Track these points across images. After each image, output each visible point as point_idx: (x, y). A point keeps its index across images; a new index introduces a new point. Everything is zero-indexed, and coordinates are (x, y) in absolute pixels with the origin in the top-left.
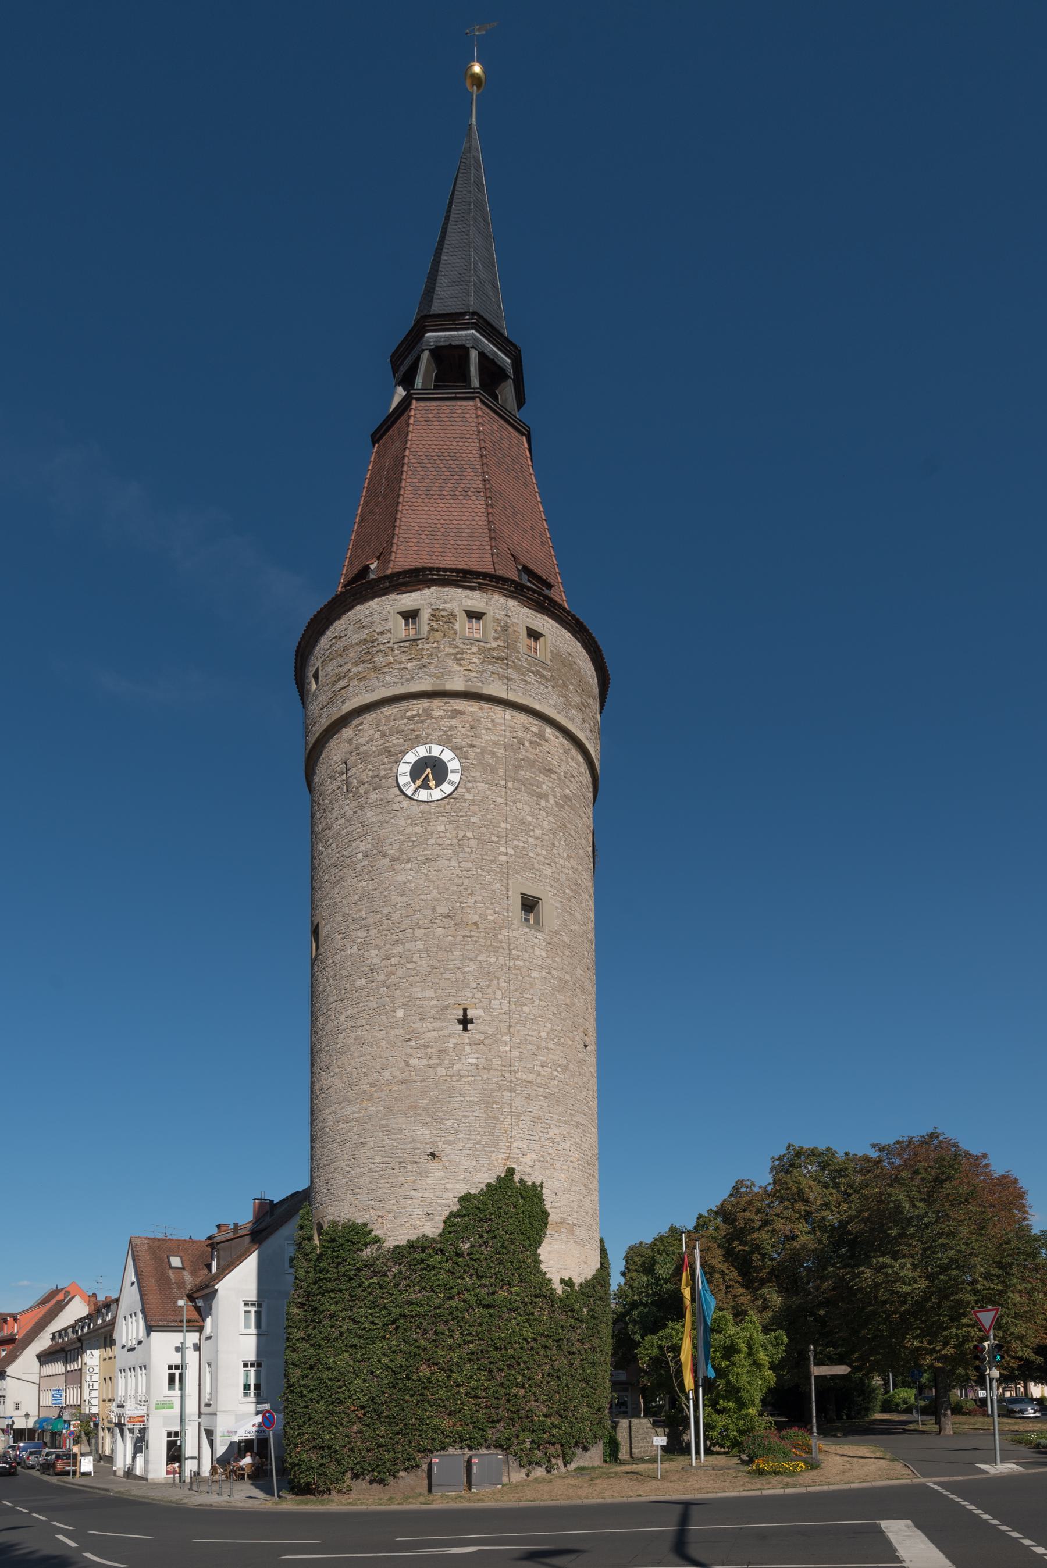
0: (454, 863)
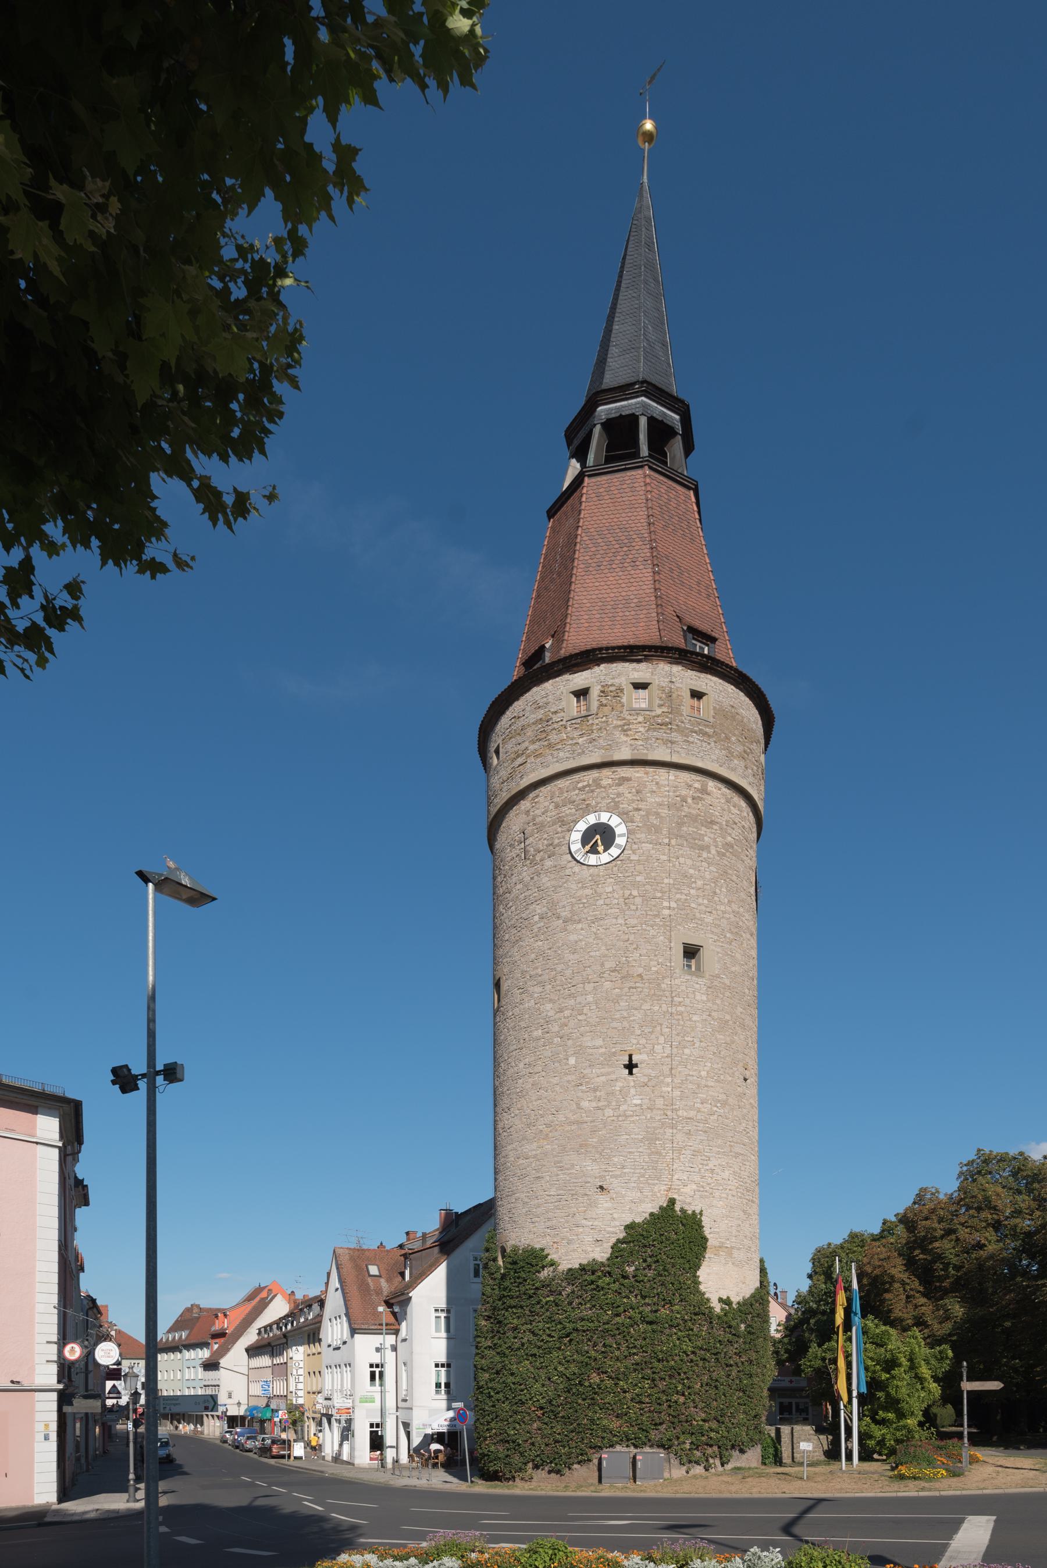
0: (621, 921)
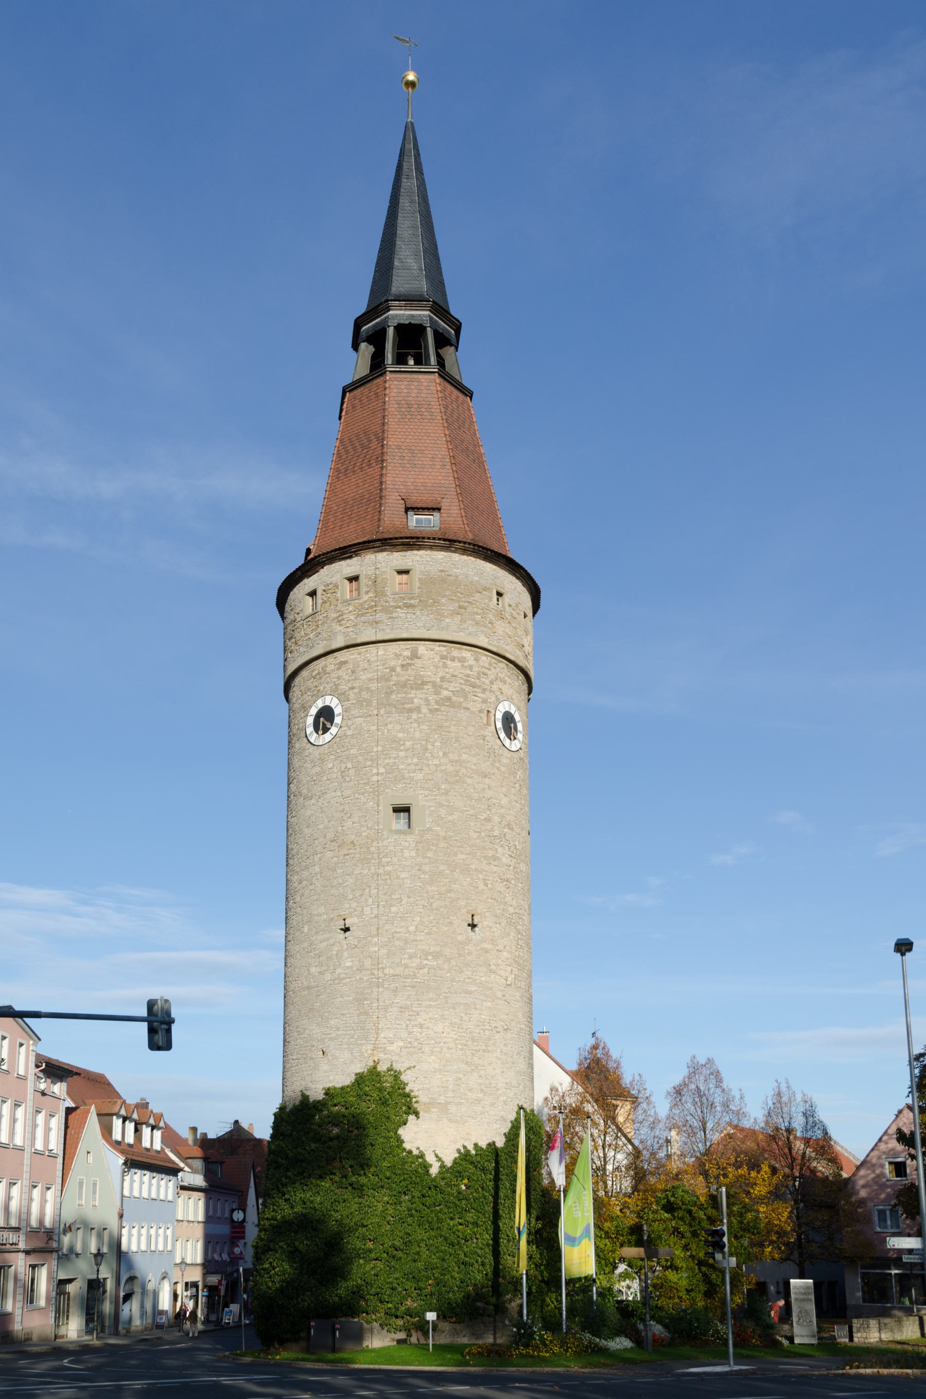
0: (339, 793)
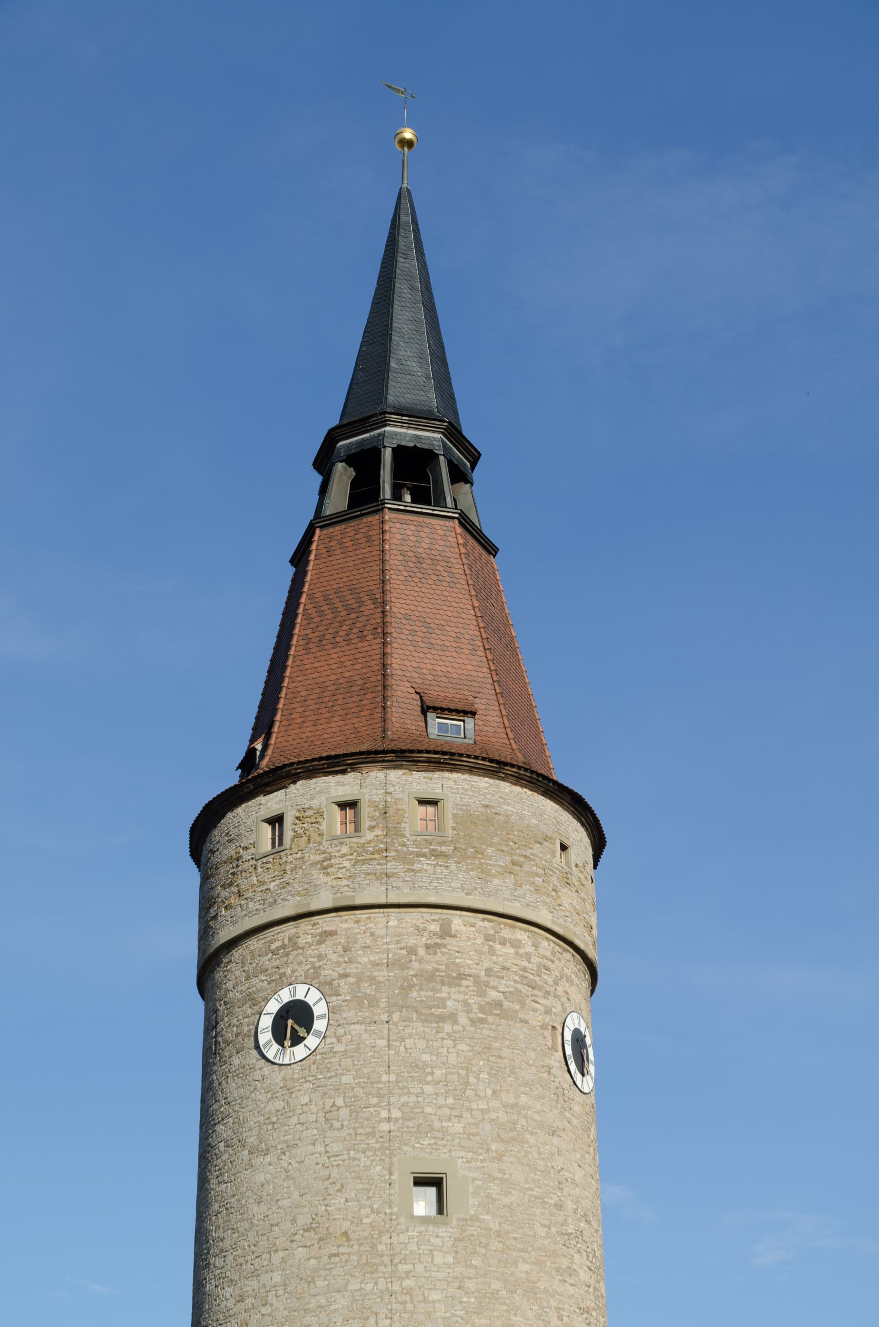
0: (320, 1148)
